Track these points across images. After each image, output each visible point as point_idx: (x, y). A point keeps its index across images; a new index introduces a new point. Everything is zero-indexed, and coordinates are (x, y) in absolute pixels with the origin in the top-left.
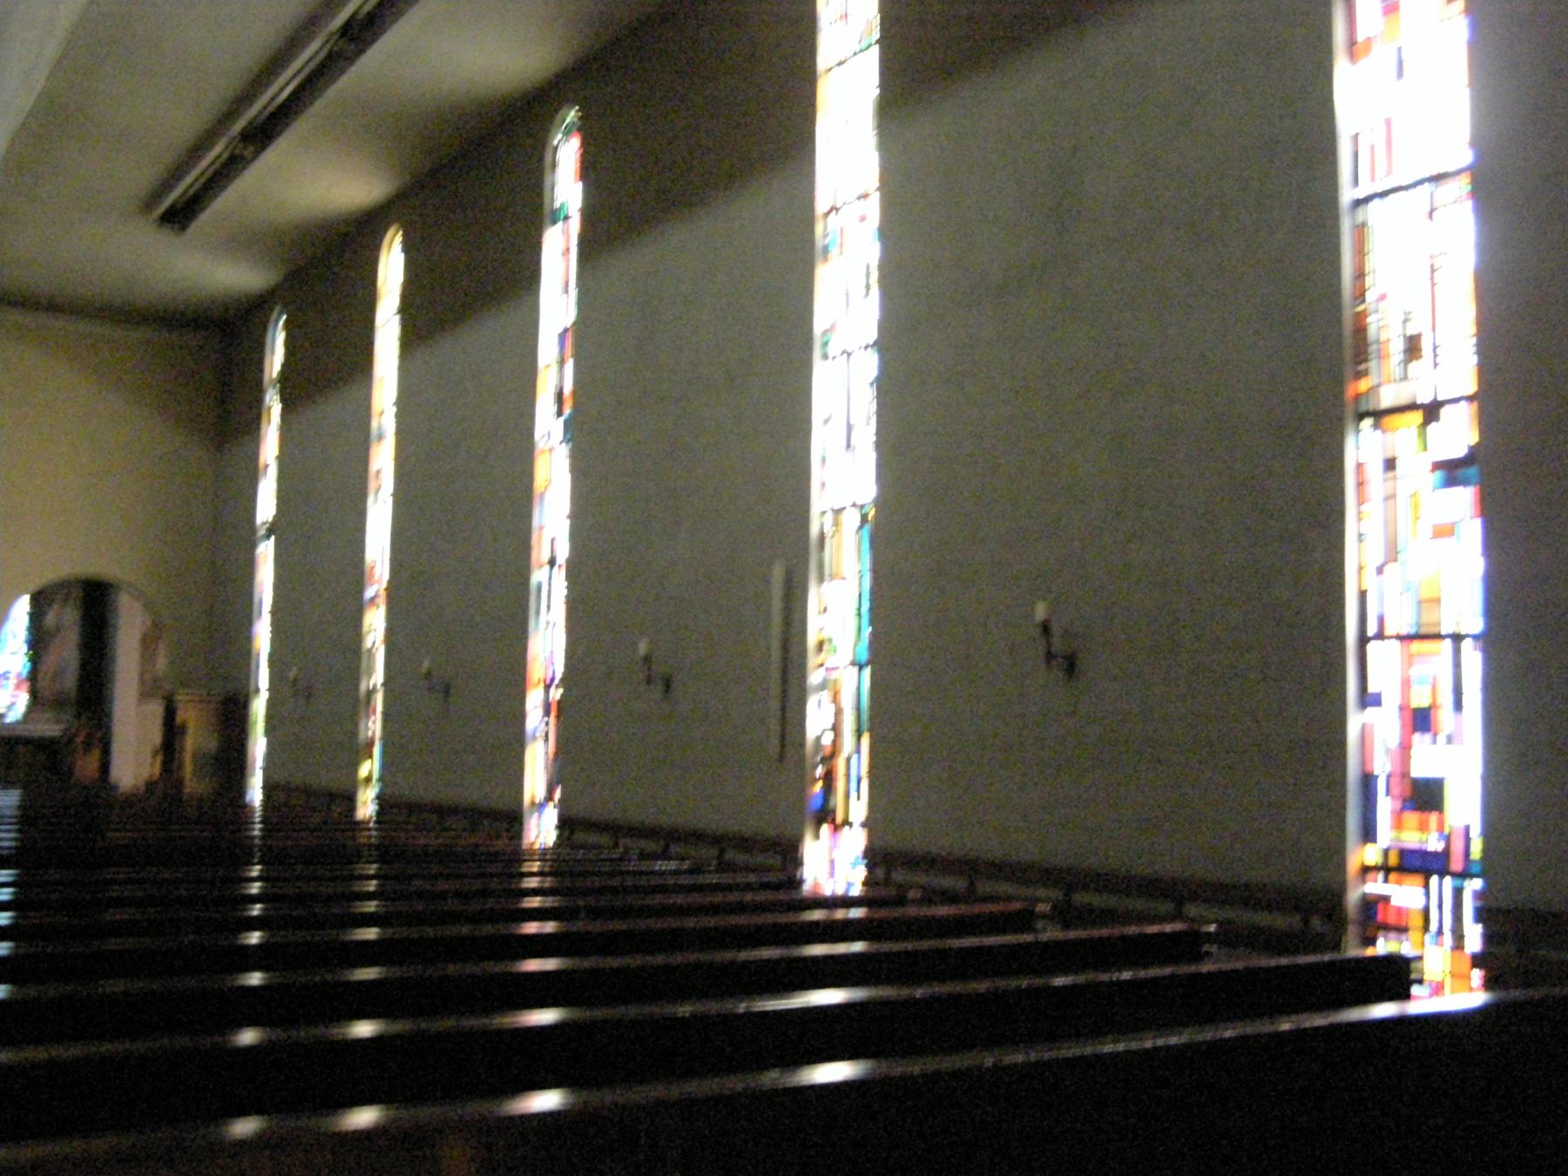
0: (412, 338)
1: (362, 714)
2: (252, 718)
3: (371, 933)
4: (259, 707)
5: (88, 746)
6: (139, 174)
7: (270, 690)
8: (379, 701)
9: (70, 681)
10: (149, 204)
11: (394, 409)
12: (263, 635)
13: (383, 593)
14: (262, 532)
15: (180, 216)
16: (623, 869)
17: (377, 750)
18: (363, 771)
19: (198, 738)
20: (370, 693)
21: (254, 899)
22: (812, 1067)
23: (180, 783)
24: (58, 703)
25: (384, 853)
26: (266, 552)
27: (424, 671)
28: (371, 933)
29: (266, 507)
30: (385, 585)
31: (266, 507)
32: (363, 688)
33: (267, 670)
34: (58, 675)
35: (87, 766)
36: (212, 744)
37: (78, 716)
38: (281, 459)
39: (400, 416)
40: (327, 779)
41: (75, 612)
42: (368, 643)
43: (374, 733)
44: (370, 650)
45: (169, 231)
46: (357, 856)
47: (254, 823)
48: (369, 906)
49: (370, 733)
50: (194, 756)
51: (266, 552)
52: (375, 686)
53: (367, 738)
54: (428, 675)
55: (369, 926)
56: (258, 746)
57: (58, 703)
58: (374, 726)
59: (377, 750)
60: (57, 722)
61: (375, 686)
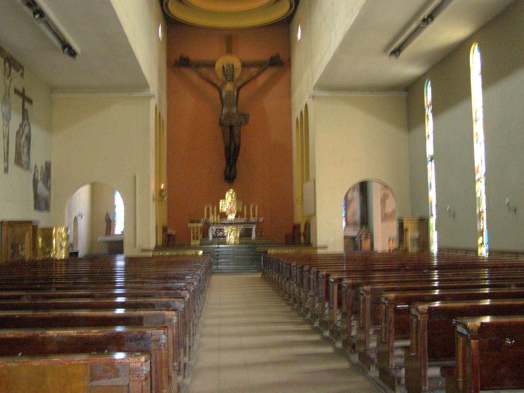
0: (486, 84)
1: (478, 221)
2: (431, 225)
3: (487, 302)
4: (433, 221)
5: (366, 238)
6: (384, 39)
7: (436, 214)
8: (484, 215)
9: (358, 217)
10: (386, 50)
11: (482, 110)
12: (432, 195)
13: (483, 176)
14: (429, 159)
15: (397, 52)
16: (246, 249)
17: (485, 233)
18: (480, 241)
19: (412, 234)
20: (480, 213)
21: (436, 288)
22: (484, 317)
23: (406, 250)
24: (355, 224)
25: (440, 268)
26: (431, 167)
27: (506, 203)
28: (487, 302)
29: (430, 150)
30: (484, 173)
31: (430, 150)
32: (478, 211)
33: (435, 208)
34: (354, 214)
35: (366, 245)
36: (416, 235)
37: (361, 228)
38: (434, 132)
39: (484, 112)
40: (469, 245)
41: (358, 193)
42: (478, 195)
43: (483, 227)
44: (479, 198)
45: (394, 57)
46: (432, 268)
47: (434, 261)
48: (486, 290)
49: (482, 228)
50: (411, 239)
51: (431, 167)
52: (482, 210)
53: (480, 229)
54: (508, 204)
55: (487, 299)
56: (434, 235)
57: (355, 224)
58: (483, 225)
59: (485, 233)
60: (354, 230)
61: (482, 210)
